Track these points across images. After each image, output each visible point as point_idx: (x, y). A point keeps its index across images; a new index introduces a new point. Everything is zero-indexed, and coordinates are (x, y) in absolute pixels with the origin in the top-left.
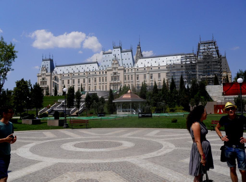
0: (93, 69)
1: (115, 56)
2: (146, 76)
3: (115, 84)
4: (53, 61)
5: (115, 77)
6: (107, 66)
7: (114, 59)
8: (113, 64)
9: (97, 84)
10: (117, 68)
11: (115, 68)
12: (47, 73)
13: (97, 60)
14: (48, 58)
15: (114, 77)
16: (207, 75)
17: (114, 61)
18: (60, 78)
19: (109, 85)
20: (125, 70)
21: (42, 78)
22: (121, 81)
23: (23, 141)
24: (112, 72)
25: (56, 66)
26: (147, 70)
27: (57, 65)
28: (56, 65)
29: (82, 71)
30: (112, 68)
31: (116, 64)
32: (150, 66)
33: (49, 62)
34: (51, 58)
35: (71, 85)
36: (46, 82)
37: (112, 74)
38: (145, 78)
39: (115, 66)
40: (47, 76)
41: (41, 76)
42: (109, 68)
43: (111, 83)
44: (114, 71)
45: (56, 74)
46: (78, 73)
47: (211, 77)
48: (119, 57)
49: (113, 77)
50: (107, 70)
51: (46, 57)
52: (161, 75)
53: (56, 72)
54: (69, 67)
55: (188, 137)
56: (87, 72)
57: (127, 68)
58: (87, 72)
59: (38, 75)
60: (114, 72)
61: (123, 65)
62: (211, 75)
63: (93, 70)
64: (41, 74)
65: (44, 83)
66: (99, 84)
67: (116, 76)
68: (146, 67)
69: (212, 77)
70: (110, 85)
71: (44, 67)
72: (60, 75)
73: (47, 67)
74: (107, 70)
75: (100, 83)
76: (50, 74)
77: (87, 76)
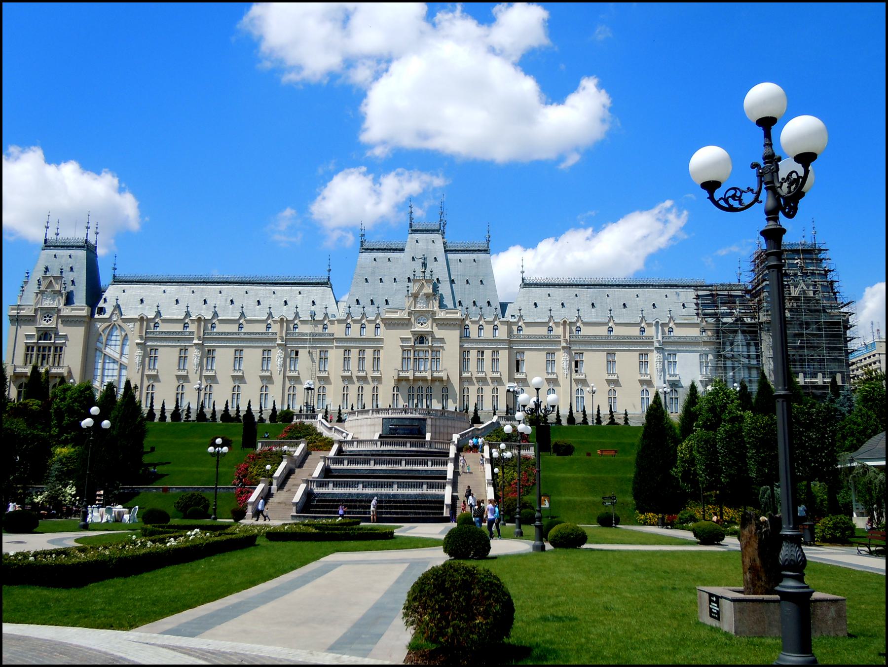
0: (313, 308)
1: (424, 265)
2: (188, 354)
3: (420, 383)
5: (44, 348)
6: (379, 301)
7: (419, 275)
8: (415, 296)
9: (161, 377)
10: (59, 310)
11: (421, 316)
12: (69, 308)
14: (79, 235)
16: (805, 374)
17: (418, 285)
18: (141, 338)
19: (393, 384)
20: (466, 328)
21: (38, 330)
22: (448, 377)
24: (31, 330)
25: (117, 281)
26: (276, 333)
27: (120, 273)
28: (117, 273)
30: (410, 314)
31: (427, 296)
32: (292, 318)
33: (82, 254)
34: (92, 239)
36: (59, 349)
37: (408, 339)
38: (182, 362)
39: (421, 306)
41: (30, 320)
42: (395, 310)
43: (400, 380)
44: (44, 324)
45: (115, 318)
46: (639, 324)
47: (820, 383)
48: (439, 270)
50: (383, 320)
52: (244, 354)
53: (118, 307)
54: (187, 289)
56: (282, 319)
57: (359, 318)
59: (14, 313)
60: (416, 329)
61: (457, 304)
62: (820, 375)
63: (313, 315)
64: (36, 310)
65: (43, 356)
66: (344, 378)
67: (50, 348)
68: (275, 322)
69: (824, 382)
71: (55, 278)
72: (138, 324)
73: (68, 276)
74: (383, 320)
75: (348, 374)
76: (84, 313)
77: (282, 338)
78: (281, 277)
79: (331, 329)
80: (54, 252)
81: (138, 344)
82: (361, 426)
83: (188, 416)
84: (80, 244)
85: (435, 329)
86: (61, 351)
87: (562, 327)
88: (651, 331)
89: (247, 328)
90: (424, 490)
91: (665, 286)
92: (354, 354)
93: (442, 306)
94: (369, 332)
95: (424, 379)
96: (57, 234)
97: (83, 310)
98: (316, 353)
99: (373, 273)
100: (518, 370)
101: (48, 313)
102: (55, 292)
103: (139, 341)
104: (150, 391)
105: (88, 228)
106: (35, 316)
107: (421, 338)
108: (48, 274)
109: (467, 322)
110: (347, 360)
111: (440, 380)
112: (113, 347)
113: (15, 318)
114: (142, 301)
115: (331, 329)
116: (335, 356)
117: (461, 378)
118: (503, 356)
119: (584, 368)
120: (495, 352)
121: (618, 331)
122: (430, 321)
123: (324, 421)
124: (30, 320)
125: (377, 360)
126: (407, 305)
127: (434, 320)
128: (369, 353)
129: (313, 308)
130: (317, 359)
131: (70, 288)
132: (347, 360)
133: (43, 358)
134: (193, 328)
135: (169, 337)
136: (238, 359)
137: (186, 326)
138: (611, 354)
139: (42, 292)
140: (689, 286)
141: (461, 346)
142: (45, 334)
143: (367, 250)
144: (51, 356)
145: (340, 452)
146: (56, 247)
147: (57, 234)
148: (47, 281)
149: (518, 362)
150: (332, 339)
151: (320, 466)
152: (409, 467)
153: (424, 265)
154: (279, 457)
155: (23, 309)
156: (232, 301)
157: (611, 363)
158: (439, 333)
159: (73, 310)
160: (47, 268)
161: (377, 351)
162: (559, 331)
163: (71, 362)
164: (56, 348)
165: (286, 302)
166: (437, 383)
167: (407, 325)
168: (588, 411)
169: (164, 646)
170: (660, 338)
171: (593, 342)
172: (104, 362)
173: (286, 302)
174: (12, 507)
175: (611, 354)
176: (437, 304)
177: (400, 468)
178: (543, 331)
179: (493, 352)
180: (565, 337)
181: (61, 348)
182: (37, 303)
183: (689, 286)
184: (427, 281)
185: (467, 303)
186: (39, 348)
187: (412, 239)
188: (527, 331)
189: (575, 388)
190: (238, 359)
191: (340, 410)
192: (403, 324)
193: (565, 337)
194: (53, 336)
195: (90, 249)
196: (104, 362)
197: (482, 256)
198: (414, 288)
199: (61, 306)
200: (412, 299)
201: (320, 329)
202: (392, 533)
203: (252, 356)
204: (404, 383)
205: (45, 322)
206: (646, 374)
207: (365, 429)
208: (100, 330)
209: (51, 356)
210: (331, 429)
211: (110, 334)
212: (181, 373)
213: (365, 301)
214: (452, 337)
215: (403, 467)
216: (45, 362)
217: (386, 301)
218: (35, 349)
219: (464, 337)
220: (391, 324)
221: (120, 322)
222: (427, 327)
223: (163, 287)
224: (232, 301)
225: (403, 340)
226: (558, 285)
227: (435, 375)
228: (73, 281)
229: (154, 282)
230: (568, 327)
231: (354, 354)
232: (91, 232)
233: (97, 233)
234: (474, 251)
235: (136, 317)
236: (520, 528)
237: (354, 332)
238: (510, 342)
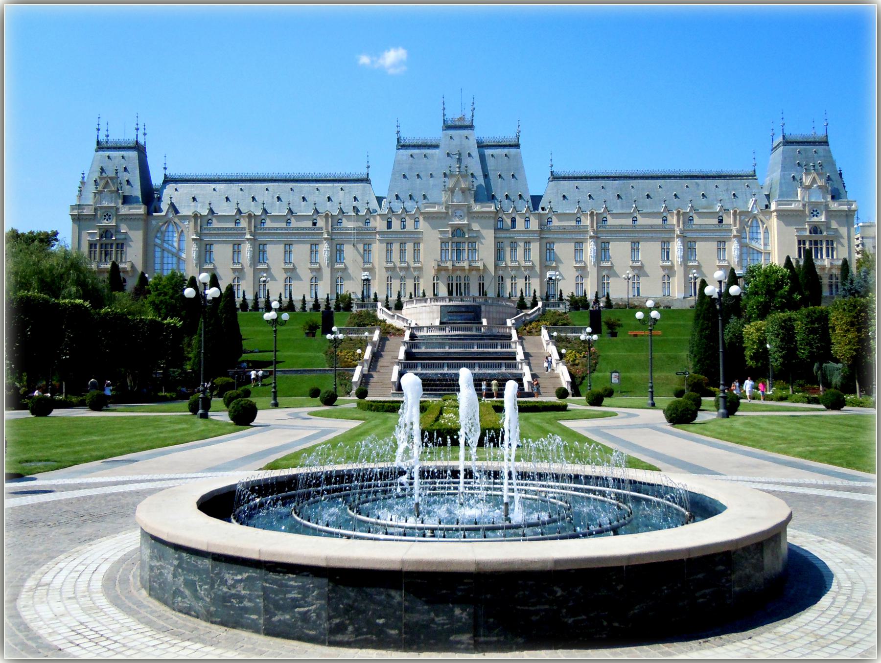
0: (355, 204)
1: (459, 160)
3: (458, 273)
4: (147, 150)
5: (816, 243)
6: (418, 196)
8: (452, 191)
13: (368, 167)
14: (129, 137)
15: (810, 242)
22: (484, 265)
23: (144, 486)
27: (172, 172)
28: (553, 169)
29: (225, 210)
34: (141, 141)
35: (846, 256)
40: (128, 218)
42: (434, 204)
43: (440, 269)
49: (114, 247)
51: (401, 129)
54: (235, 187)
55: (27, 613)
56: (250, 215)
58: (250, 215)
64: (95, 209)
70: (437, 277)
71: (111, 178)
73: (124, 176)
79: (373, 224)
80: (107, 153)
81: (194, 240)
82: (420, 313)
83: (303, 308)
84: (131, 145)
86: (122, 248)
87: (589, 218)
89: (294, 224)
90: (445, 371)
91: (687, 177)
92: (396, 247)
95: (462, 269)
96: (107, 136)
97: (140, 208)
98: (360, 247)
99: (411, 169)
103: (194, 237)
105: (137, 129)
106: (95, 215)
107: (458, 231)
108: (104, 175)
110: (389, 251)
111: (477, 269)
114: (194, 199)
116: (378, 249)
118: (535, 247)
120: (527, 243)
123: (385, 309)
125: (416, 251)
126: (444, 199)
127: (117, 216)
128: (409, 247)
129: (355, 204)
132: (389, 251)
133: (106, 255)
134: (244, 224)
135: (223, 234)
136: (288, 252)
137: (237, 222)
138: (635, 242)
139: (100, 192)
142: (106, 233)
143: (404, 147)
144: (114, 252)
145: (413, 336)
146: (109, 148)
147: (107, 136)
151: (402, 350)
152: (480, 350)
153: (459, 160)
154: (363, 344)
156: (279, 198)
157: (635, 250)
160: (102, 169)
161: (417, 243)
163: (133, 257)
165: (329, 199)
166: (474, 272)
168: (308, 298)
169: (763, 491)
171: (619, 233)
172: (163, 257)
173: (329, 199)
175: (635, 242)
177: (472, 350)
179: (525, 242)
180: (592, 227)
181: (122, 244)
182: (95, 203)
184: (462, 176)
185: (500, 196)
186: (102, 245)
190: (288, 252)
191: (387, 297)
193: (592, 227)
195: (140, 149)
196: (163, 257)
197: (513, 151)
198: (450, 183)
202: (566, 406)
203: (301, 251)
204: (443, 272)
206: (581, 261)
207: (424, 316)
209: (114, 252)
210: (393, 316)
212: (389, 265)
215: (475, 350)
216: (108, 258)
217: (424, 196)
218: (98, 246)
223: (213, 186)
228: (128, 181)
231: (396, 247)
232: (141, 132)
233: (145, 134)
234: (505, 146)
235: (190, 214)
236: (652, 399)
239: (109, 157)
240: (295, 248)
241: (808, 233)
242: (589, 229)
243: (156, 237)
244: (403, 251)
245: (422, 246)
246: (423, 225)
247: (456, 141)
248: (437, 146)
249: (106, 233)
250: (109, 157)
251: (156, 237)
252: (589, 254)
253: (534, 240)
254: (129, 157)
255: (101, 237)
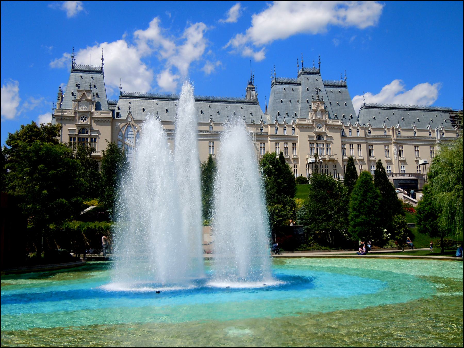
5: (83, 139)
10: (92, 113)
11: (320, 123)
12: (99, 112)
21: (78, 126)
28: (122, 90)
30: (313, 121)
31: (322, 111)
50: (296, 125)
60: (317, 131)
64: (75, 113)
67: (87, 139)
71: (87, 91)
74: (296, 125)
78: (214, 97)
79: (265, 130)
85: (328, 131)
88: (434, 134)
93: (330, 118)
94: (289, 132)
97: (109, 114)
99: (285, 97)
100: (370, 155)
101: (84, 115)
102: (88, 101)
104: (418, 169)
106: (74, 117)
107: (319, 136)
109: (343, 127)
112: (129, 139)
113: (59, 118)
115: (265, 130)
117: (343, 159)
118: (364, 147)
119: (404, 154)
121: (419, 134)
122: (89, 118)
124: (71, 119)
125: (294, 148)
127: (92, 118)
130: (259, 148)
131: (97, 100)
138: (416, 146)
140: (445, 111)
141: (342, 141)
142: (83, 129)
146: (81, 71)
148: (81, 94)
149: (370, 150)
150: (267, 136)
155: (66, 112)
156: (202, 111)
158: (95, 127)
159: (101, 113)
161: (294, 143)
162: (390, 133)
164: (91, 139)
166: (330, 163)
167: (311, 128)
170: (395, 137)
171: (408, 140)
174: (31, 255)
175: (416, 146)
176: (327, 116)
178: (382, 133)
179: (276, 143)
181: (95, 139)
182: (75, 108)
183: (445, 111)
187: (305, 77)
188: (373, 133)
189: (400, 165)
192: (309, 128)
194: (89, 131)
197: (343, 89)
199: (93, 110)
200: (313, 112)
201: (259, 130)
205: (82, 121)
206: (389, 157)
208: (121, 126)
211: (127, 130)
213: (283, 114)
214: (337, 136)
218: (89, 139)
219: (343, 136)
220: (303, 127)
221: (133, 123)
222: (323, 130)
223: (156, 102)
224: (202, 111)
225: (309, 137)
226: (383, 108)
227: (331, 157)
229: (219, 101)
230: (394, 131)
237: (280, 132)
238: (366, 139)
239: (81, 77)
240: (405, 148)
241: (315, 139)
242: (392, 138)
243: (119, 134)
244: (351, 149)
245: (298, 145)
246: (297, 132)
247: (311, 81)
248: (300, 84)
249: (83, 129)
250: (81, 77)
251: (119, 134)
252: (393, 153)
253: (363, 143)
254: (97, 78)
255: (79, 132)
